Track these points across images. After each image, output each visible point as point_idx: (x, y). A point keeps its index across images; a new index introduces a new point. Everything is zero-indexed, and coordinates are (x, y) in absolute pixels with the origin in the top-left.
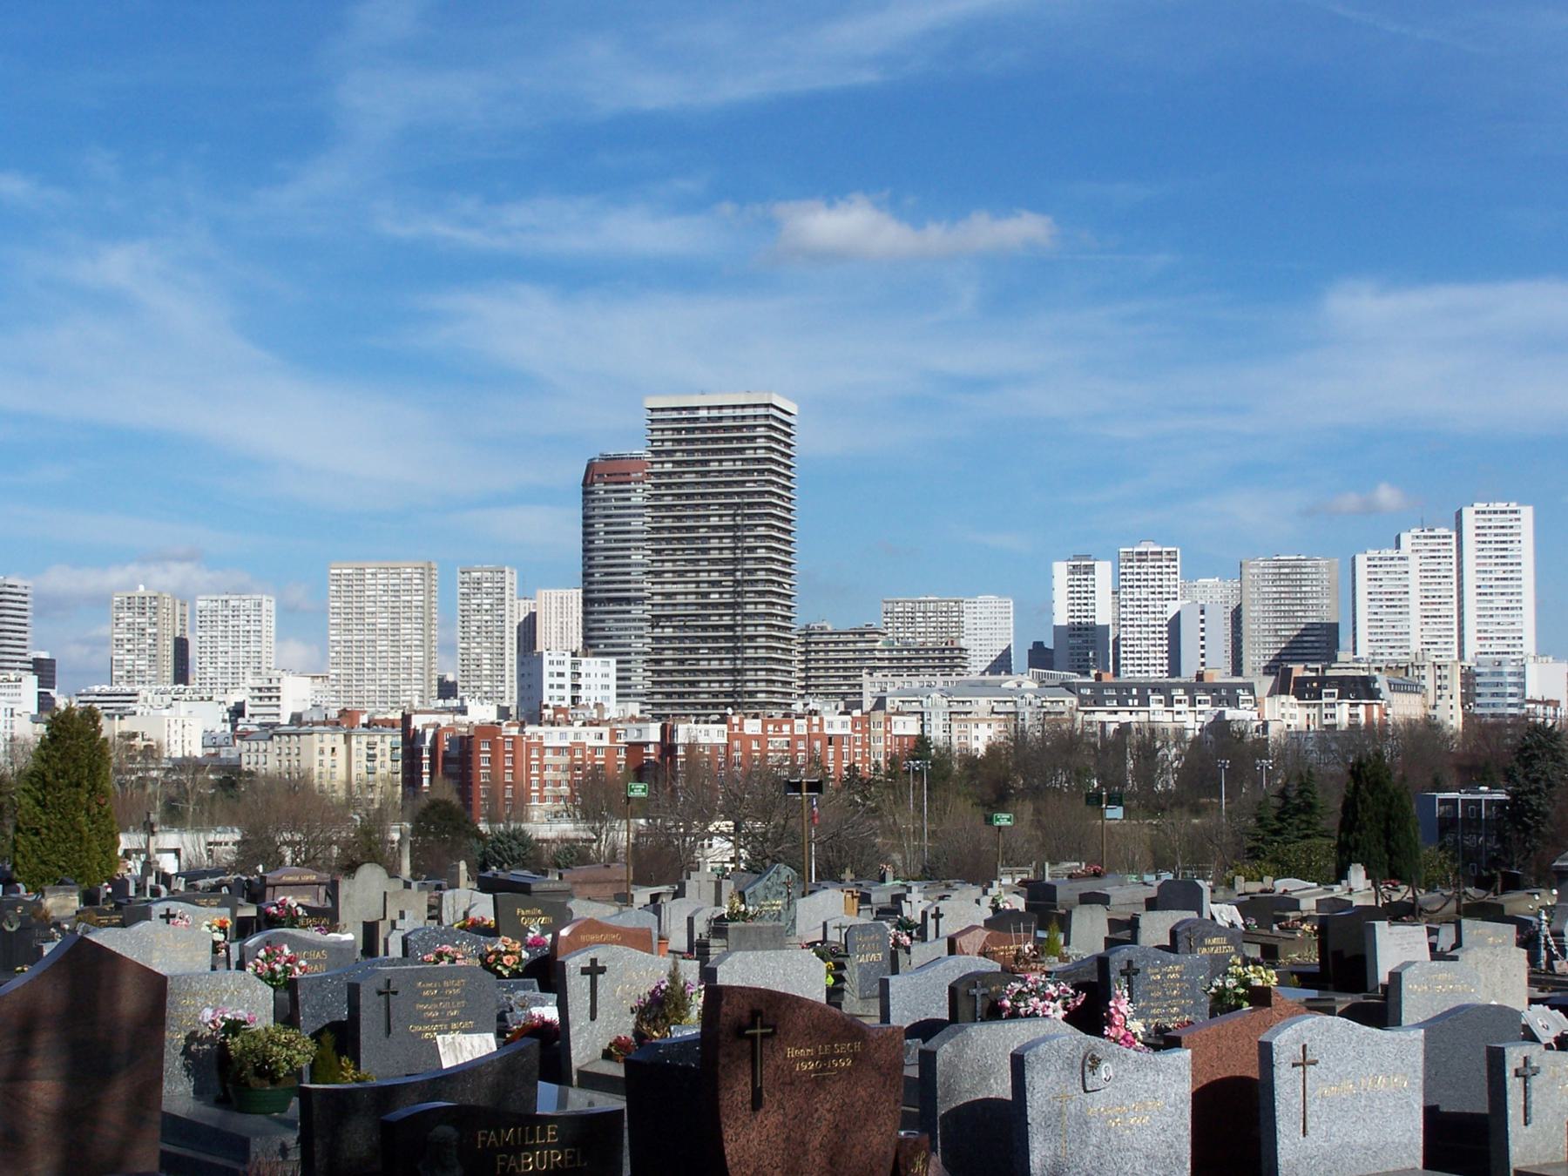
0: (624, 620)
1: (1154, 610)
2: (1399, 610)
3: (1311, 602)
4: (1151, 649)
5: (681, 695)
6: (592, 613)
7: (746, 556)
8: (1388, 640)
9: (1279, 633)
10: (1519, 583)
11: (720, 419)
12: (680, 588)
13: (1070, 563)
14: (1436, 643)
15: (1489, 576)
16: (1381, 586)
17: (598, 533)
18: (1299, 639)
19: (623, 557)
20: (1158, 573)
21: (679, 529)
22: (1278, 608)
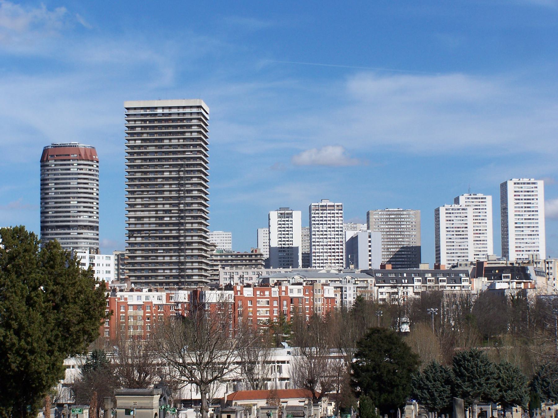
0: (66, 238)
1: (330, 236)
2: (462, 237)
3: (406, 233)
4: (329, 258)
5: (147, 277)
6: (47, 234)
7: (186, 195)
8: (457, 253)
9: (389, 250)
10: (537, 221)
11: (170, 114)
12: (146, 214)
13: (279, 212)
14: (478, 255)
15: (521, 217)
16: (453, 224)
17: (51, 188)
18: (400, 253)
19: (66, 202)
20: (332, 217)
21: (145, 179)
22: (389, 237)
